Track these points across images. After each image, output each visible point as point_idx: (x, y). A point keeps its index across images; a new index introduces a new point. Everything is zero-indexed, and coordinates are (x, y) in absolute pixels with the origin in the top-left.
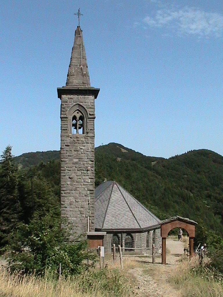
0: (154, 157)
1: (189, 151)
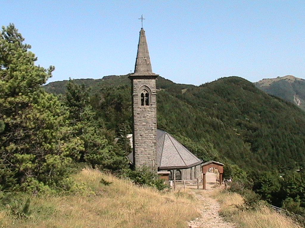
0: (184, 85)
1: (219, 78)
